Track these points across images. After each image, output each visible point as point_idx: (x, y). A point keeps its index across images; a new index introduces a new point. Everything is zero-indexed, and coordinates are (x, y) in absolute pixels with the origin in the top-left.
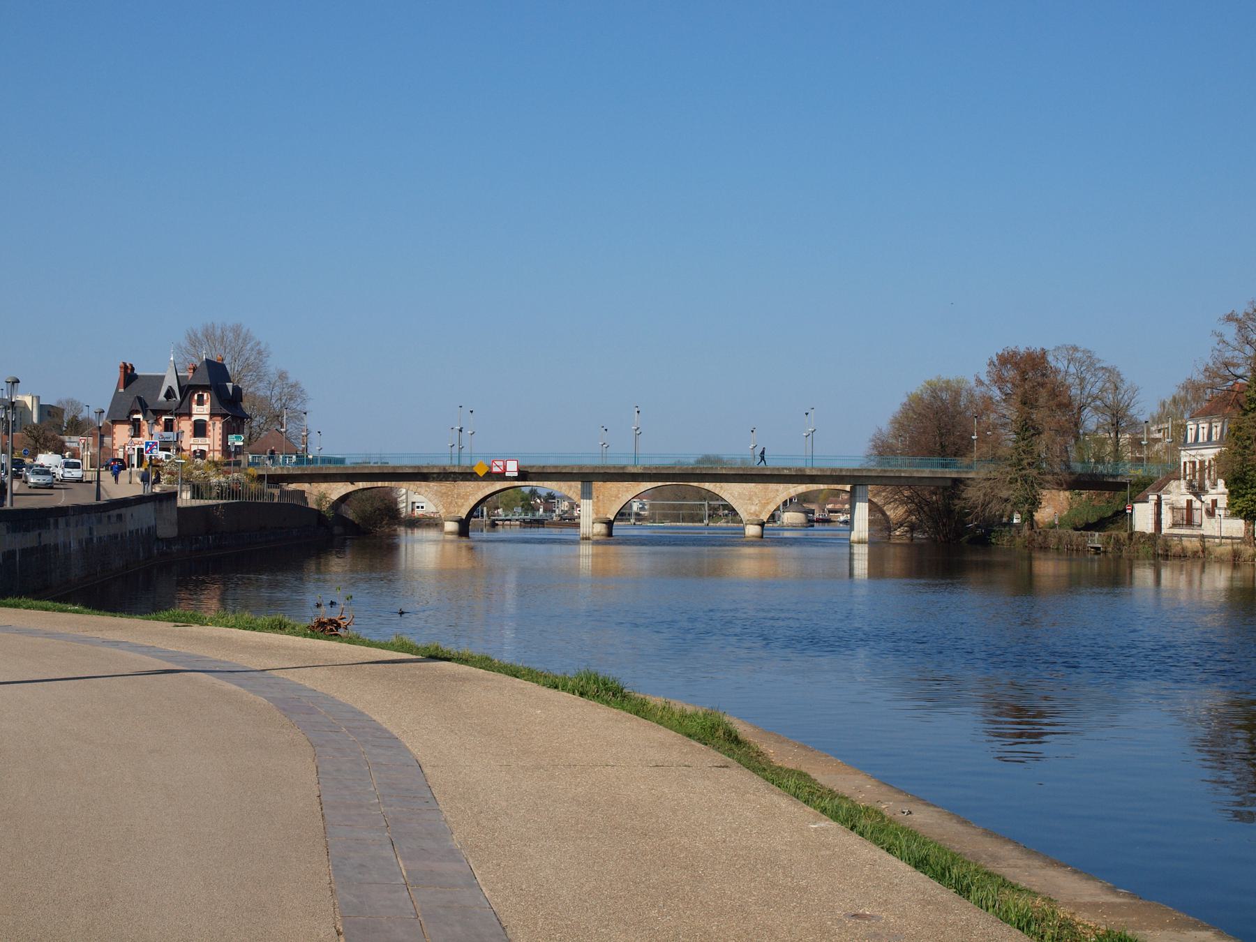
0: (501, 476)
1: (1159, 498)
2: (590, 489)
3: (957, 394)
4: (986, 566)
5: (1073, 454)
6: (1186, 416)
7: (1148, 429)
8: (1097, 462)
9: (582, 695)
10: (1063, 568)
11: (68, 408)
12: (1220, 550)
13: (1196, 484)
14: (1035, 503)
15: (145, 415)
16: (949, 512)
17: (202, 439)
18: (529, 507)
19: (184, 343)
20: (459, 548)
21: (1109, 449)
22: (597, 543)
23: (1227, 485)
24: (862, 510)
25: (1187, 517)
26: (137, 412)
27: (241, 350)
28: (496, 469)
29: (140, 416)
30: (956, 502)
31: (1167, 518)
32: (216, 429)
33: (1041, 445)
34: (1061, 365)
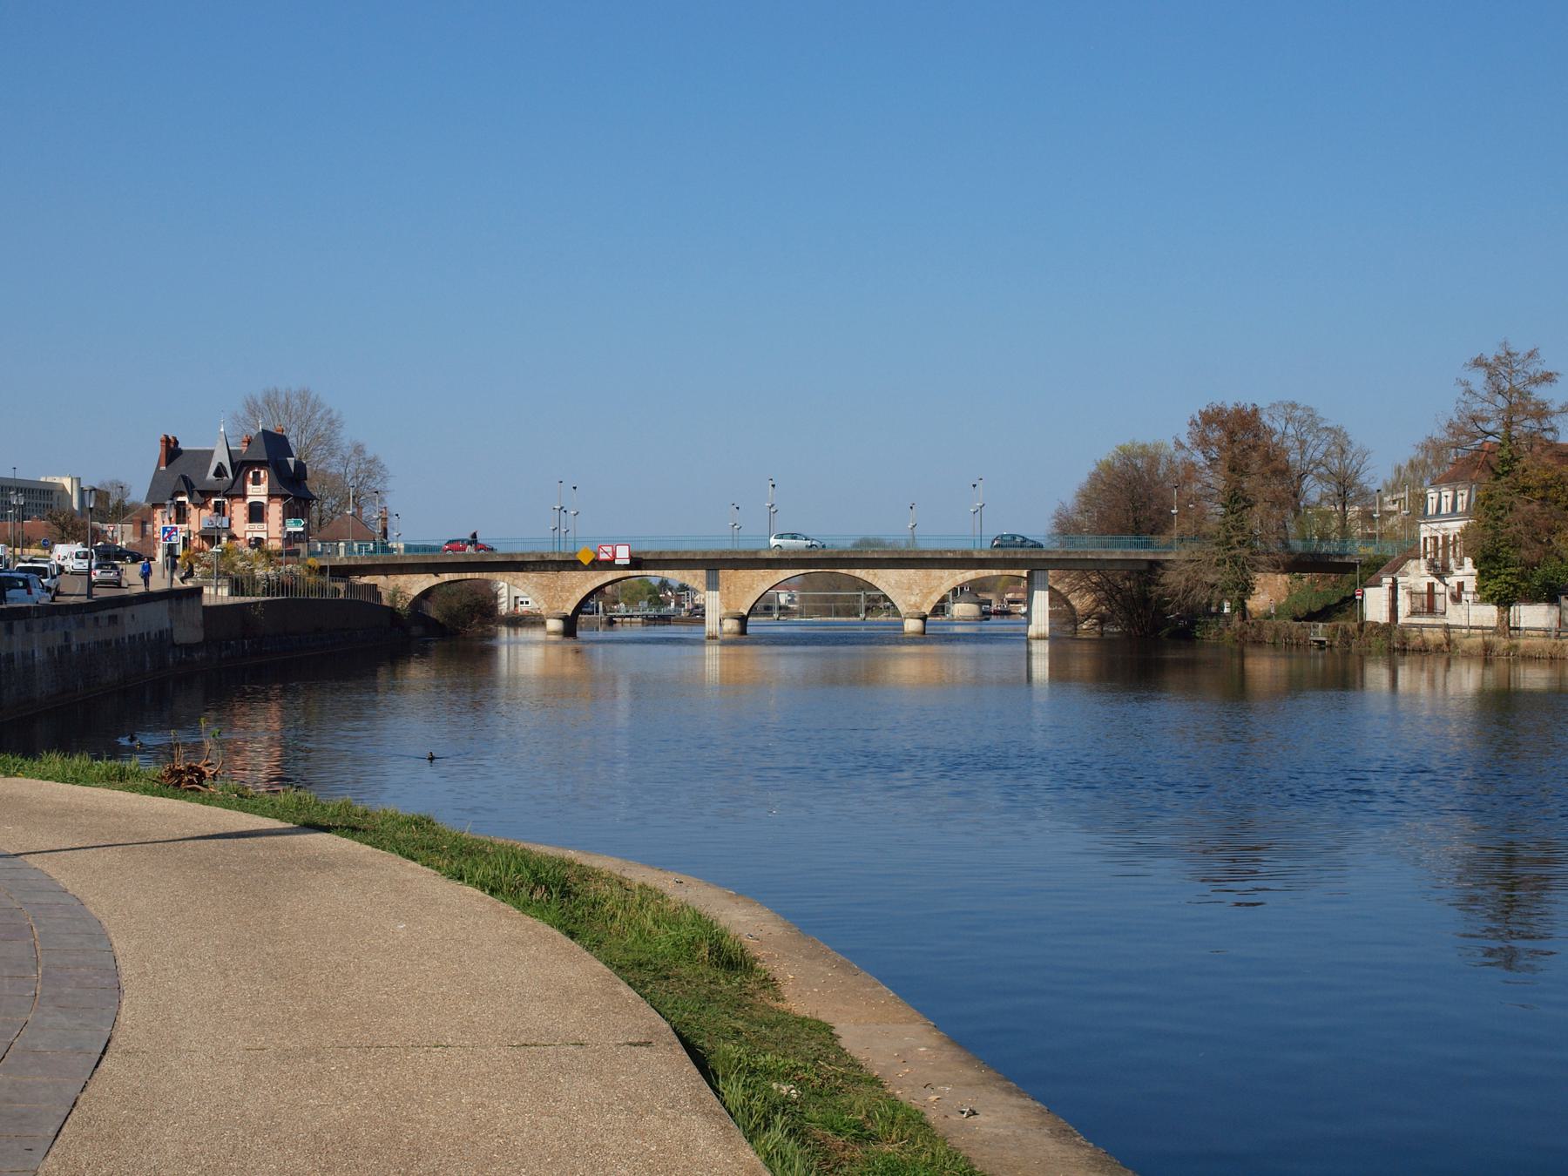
0: (610, 565)
1: (1395, 582)
2: (717, 577)
3: (1154, 460)
4: (1190, 665)
5: (1293, 530)
6: (1426, 483)
7: (1381, 500)
8: (1321, 539)
9: (493, 892)
10: (1282, 666)
11: (112, 492)
12: (1467, 643)
13: (1438, 563)
14: (1247, 589)
15: (191, 498)
16: (1145, 601)
17: (259, 525)
18: (659, 602)
19: (242, 412)
20: (564, 652)
21: (1335, 524)
22: (724, 643)
23: (1475, 564)
24: (1041, 599)
25: (1428, 604)
26: (182, 494)
27: (309, 419)
28: (603, 556)
29: (185, 499)
30: (1154, 588)
31: (1404, 605)
32: (275, 510)
33: (1254, 520)
34: (1278, 426)
